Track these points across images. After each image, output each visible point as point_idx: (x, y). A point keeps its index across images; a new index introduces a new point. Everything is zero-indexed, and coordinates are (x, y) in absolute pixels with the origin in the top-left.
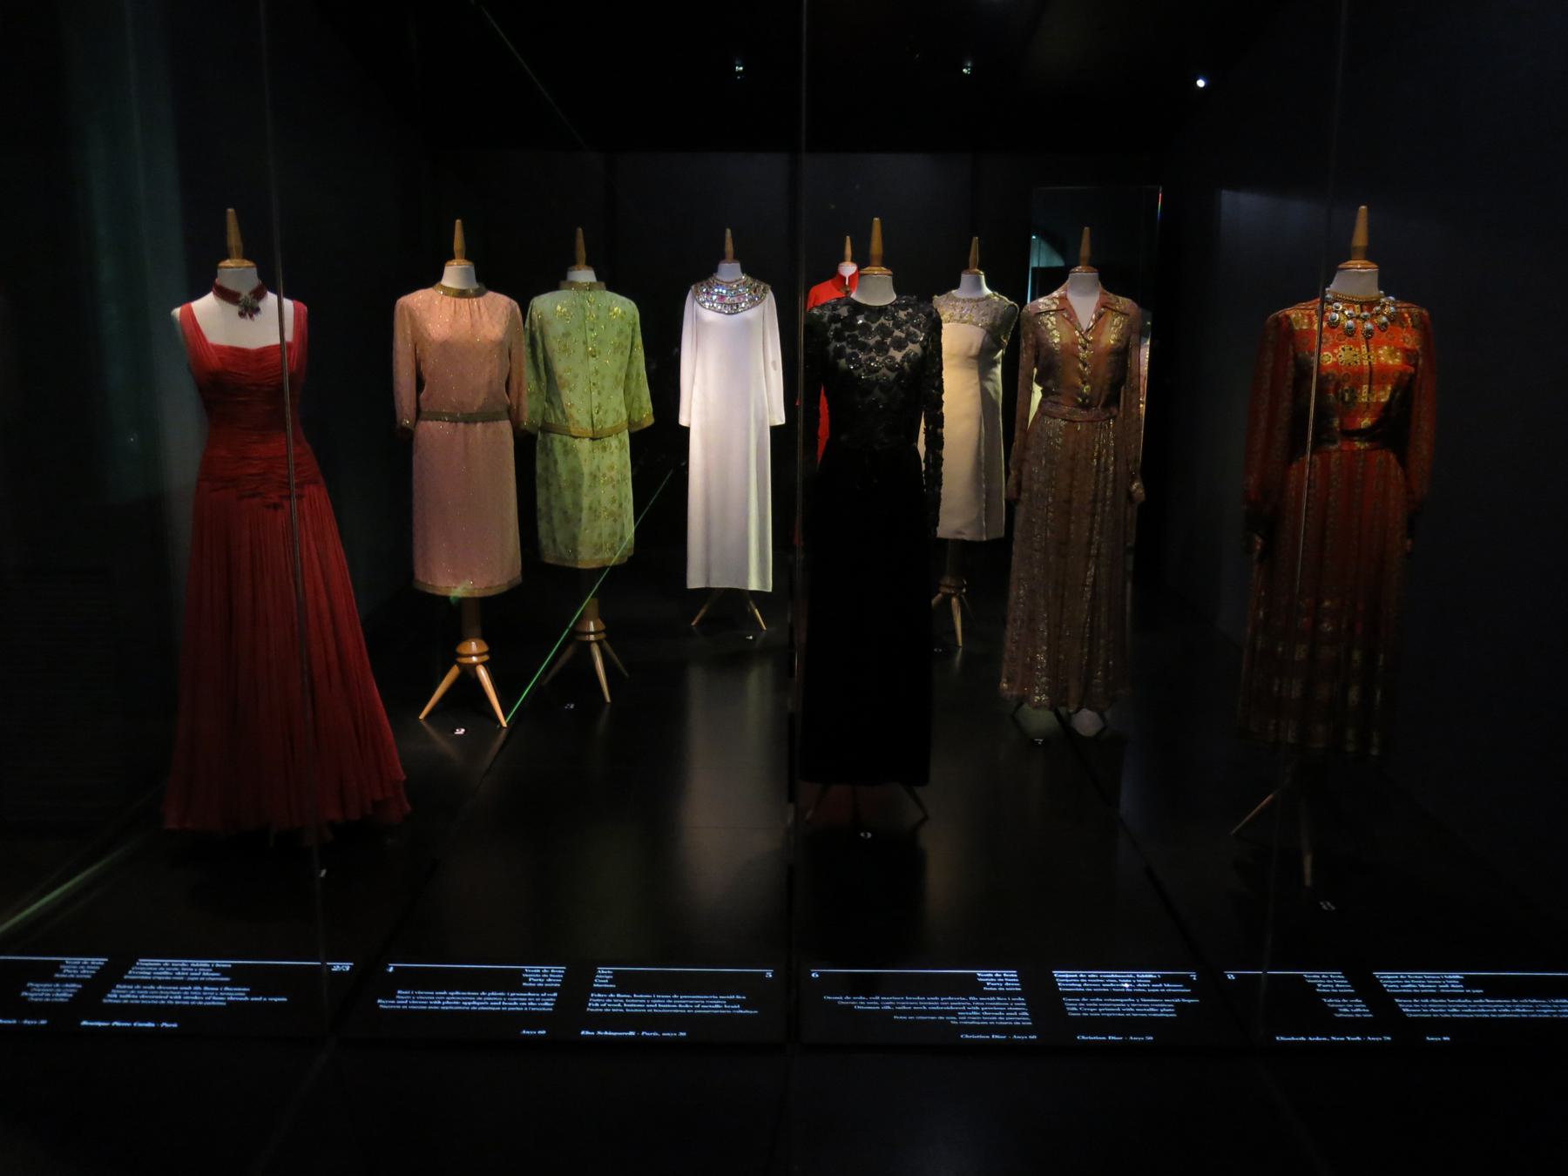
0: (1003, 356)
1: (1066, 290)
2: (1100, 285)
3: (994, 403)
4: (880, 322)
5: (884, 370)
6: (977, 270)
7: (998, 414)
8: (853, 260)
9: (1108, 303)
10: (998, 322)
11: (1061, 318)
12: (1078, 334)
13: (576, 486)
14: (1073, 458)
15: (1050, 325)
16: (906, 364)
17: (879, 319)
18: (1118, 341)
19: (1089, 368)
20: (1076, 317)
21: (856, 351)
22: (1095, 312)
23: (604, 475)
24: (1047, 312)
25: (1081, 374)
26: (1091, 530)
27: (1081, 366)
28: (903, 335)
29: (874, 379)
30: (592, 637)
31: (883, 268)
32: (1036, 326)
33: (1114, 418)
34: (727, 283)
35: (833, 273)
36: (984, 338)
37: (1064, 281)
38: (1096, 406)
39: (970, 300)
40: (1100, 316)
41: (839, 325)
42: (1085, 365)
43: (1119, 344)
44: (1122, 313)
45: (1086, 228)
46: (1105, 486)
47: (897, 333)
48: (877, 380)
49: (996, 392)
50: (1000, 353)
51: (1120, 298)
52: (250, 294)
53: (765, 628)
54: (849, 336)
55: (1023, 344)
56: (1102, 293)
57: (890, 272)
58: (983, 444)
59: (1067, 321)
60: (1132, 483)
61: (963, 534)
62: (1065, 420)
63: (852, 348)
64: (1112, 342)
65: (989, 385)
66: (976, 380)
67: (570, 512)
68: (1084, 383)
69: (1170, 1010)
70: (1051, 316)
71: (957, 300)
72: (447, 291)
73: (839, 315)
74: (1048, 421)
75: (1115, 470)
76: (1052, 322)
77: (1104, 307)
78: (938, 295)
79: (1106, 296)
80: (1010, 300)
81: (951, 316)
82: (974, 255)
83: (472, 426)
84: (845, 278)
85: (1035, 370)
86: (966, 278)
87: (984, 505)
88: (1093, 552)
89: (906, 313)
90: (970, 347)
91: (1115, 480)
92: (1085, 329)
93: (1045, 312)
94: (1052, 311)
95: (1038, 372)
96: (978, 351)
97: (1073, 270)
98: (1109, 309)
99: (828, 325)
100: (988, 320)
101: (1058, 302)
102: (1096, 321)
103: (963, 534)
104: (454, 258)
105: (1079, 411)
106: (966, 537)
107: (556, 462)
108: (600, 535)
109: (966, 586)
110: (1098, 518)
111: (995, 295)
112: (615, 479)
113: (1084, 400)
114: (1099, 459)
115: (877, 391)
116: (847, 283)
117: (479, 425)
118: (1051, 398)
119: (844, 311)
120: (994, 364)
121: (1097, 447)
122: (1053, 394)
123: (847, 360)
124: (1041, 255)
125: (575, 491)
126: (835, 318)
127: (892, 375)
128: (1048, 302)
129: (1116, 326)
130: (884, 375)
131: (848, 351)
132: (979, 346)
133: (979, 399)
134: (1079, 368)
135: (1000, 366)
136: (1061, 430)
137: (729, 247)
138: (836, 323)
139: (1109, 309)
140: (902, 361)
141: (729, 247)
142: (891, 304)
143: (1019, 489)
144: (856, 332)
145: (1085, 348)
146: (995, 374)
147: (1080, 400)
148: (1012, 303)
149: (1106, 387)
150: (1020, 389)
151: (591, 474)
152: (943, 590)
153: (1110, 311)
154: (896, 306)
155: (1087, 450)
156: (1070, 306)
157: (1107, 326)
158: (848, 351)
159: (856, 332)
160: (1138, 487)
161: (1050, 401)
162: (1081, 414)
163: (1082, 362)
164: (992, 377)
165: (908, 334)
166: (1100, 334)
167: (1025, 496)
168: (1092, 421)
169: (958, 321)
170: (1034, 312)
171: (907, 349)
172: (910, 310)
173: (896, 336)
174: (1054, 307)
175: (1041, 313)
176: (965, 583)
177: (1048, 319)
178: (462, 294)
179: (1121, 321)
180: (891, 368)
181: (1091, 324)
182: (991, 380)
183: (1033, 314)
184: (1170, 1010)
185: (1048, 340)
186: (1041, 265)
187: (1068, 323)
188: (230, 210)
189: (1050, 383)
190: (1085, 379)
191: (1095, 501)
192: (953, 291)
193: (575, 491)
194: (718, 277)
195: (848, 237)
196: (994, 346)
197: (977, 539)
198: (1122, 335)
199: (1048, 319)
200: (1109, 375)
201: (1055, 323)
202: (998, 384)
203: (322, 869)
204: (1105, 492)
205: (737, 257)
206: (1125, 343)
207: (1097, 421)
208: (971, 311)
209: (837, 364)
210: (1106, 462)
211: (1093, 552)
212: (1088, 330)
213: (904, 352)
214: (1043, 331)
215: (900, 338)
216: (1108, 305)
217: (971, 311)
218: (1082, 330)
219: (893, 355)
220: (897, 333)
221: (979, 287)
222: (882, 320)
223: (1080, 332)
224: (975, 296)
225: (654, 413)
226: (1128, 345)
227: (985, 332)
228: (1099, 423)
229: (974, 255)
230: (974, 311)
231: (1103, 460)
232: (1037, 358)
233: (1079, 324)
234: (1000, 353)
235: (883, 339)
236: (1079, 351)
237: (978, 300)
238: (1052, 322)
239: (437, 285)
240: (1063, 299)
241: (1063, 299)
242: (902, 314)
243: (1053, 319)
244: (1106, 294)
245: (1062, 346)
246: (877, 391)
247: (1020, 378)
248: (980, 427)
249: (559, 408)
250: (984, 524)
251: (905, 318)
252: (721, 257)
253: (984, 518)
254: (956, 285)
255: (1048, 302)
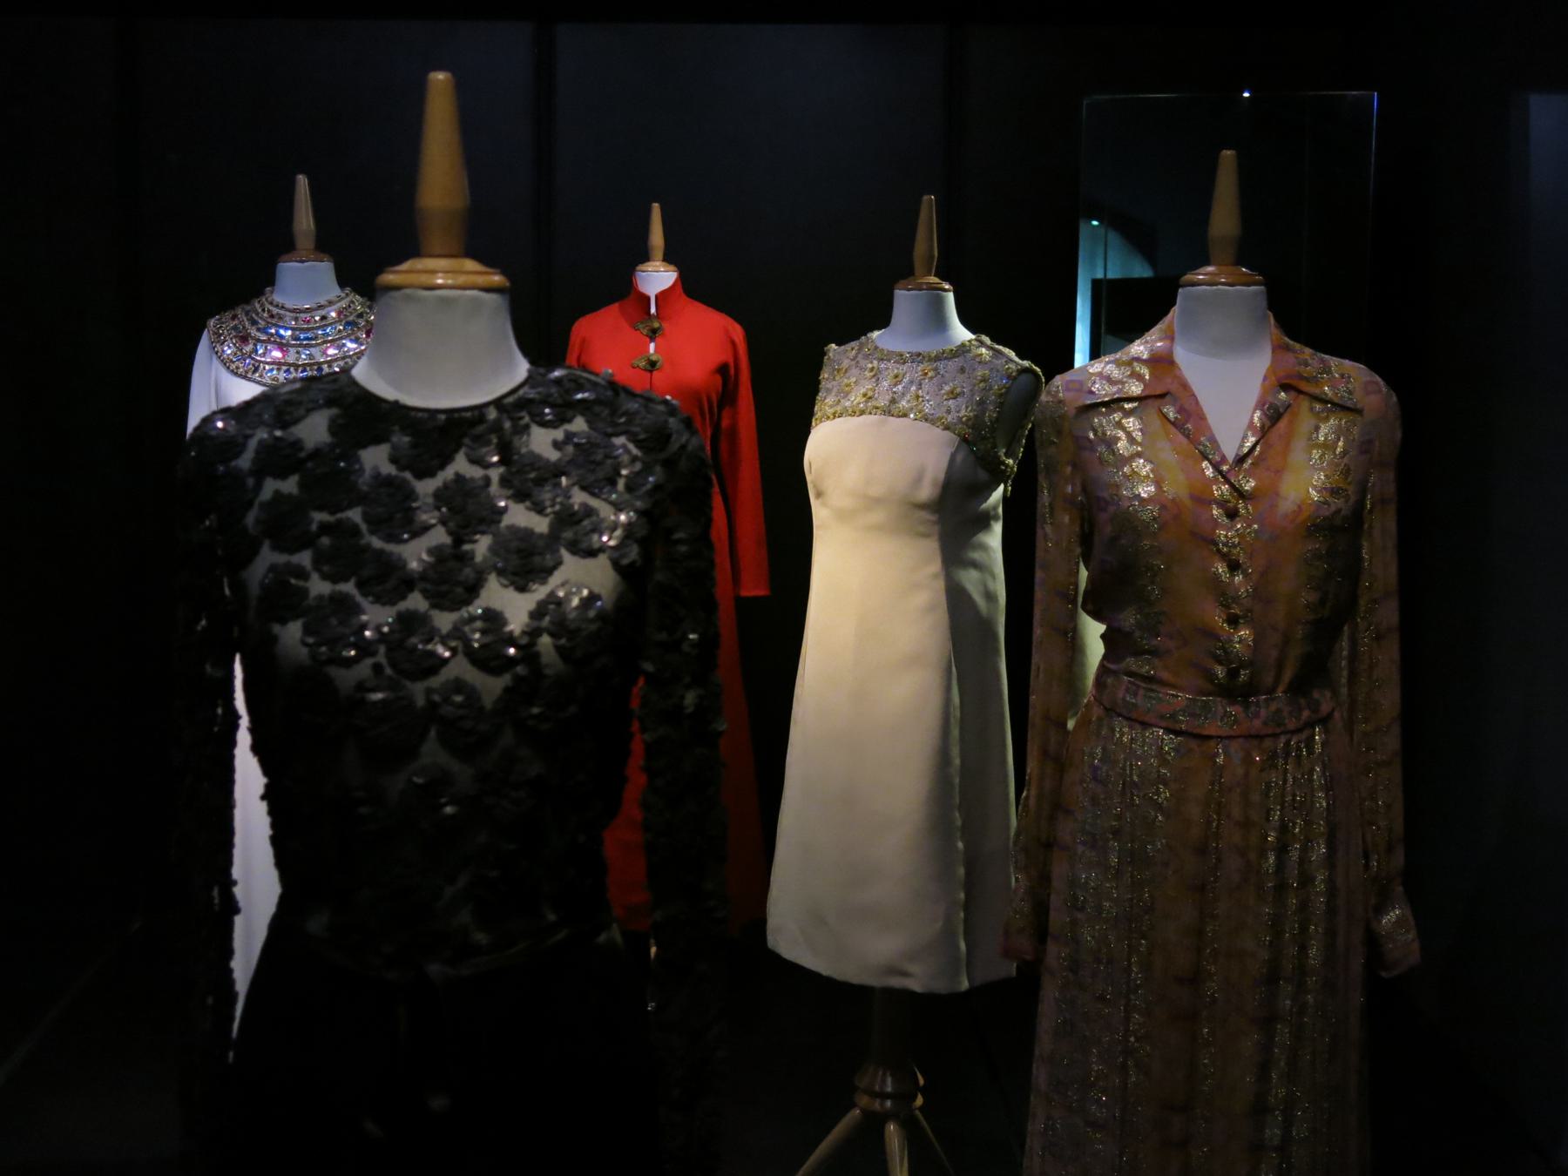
0: (1006, 499)
1: (1170, 337)
2: (1272, 321)
3: (987, 626)
4: (448, 473)
5: (461, 669)
6: (934, 279)
7: (997, 651)
8: (668, 258)
9: (1301, 377)
10: (991, 413)
11: (1156, 422)
12: (1209, 472)
14: (1202, 850)
15: (1122, 445)
16: (545, 640)
17: (446, 460)
18: (1334, 492)
19: (1246, 575)
20: (1202, 418)
21: (349, 587)
22: (1260, 405)
24: (1114, 404)
25: (1223, 595)
26: (1264, 1069)
27: (1221, 568)
28: (541, 525)
29: (420, 701)
31: (470, 264)
32: (1082, 444)
33: (1324, 721)
34: (294, 311)
35: (623, 289)
36: (953, 457)
37: (1166, 313)
38: (1271, 691)
39: (917, 357)
40: (1274, 416)
41: (290, 485)
42: (1234, 567)
43: (1338, 503)
44: (1341, 407)
45: (1228, 154)
46: (1304, 929)
47: (519, 516)
48: (432, 706)
49: (990, 597)
50: (998, 493)
51: (1334, 361)
54: (325, 528)
55: (1045, 497)
56: (1278, 348)
57: (497, 279)
58: (955, 732)
59: (1173, 429)
60: (1380, 910)
61: (905, 974)
62: (1178, 733)
63: (334, 579)
64: (1314, 495)
65: (970, 579)
66: (936, 566)
68: (1233, 621)
70: (1128, 414)
71: (885, 357)
73: (297, 444)
74: (1124, 733)
75: (1330, 882)
76: (1129, 435)
77: (1285, 387)
78: (839, 344)
79: (1290, 357)
80: (1022, 358)
81: (868, 398)
82: (926, 242)
84: (648, 299)
85: (1084, 574)
86: (904, 300)
87: (962, 896)
88: (1273, 1133)
89: (559, 434)
90: (918, 480)
91: (1331, 910)
92: (1231, 456)
93: (1104, 404)
94: (1130, 399)
95: (1090, 579)
96: (937, 491)
97: (1189, 277)
98: (1300, 392)
99: (251, 482)
100: (962, 410)
101: (1145, 372)
102: (1264, 433)
103: (905, 974)
105: (1219, 705)
106: (915, 986)
109: (924, 1091)
110: (1283, 1033)
111: (982, 344)
113: (1233, 674)
114: (1282, 849)
115: (432, 752)
116: (653, 310)
118: (1131, 663)
119: (315, 430)
120: (984, 522)
121: (1276, 816)
122: (1139, 653)
123: (307, 630)
124: (1110, 253)
126: (280, 459)
127: (491, 687)
128: (1116, 373)
129: (1328, 446)
130: (459, 685)
131: (319, 587)
132: (942, 476)
133: (942, 615)
134: (1217, 576)
135: (998, 528)
136: (1164, 762)
137: (304, 220)
138: (282, 475)
139: (1300, 392)
140: (533, 633)
141: (304, 220)
142: (498, 403)
143: (1057, 807)
144: (355, 515)
145: (1232, 514)
146: (984, 548)
147: (1220, 671)
148: (1026, 363)
149: (1299, 632)
150: (1038, 632)
152: (863, 1100)
153: (1305, 404)
154: (515, 407)
155: (1246, 824)
156: (1185, 386)
157: (1299, 444)
158: (319, 587)
159: (355, 515)
160: (1399, 922)
161: (1130, 674)
162: (1223, 717)
163: (1225, 557)
164: (976, 555)
165: (567, 519)
166: (1279, 472)
167: (1055, 953)
168: (1260, 737)
169: (887, 412)
170: (1075, 400)
171: (556, 579)
172: (579, 425)
173: (513, 529)
174: (1136, 389)
175: (1095, 406)
176: (922, 1082)
177: (1119, 425)
179: (1339, 432)
180: (488, 660)
181: (1252, 440)
182: (975, 565)
183: (1070, 410)
185: (1118, 486)
186: (1110, 275)
187: (1181, 438)
189: (1129, 619)
190: (1236, 610)
191: (1272, 978)
192: (875, 334)
194: (277, 298)
196: (983, 475)
197: (941, 986)
198: (1346, 472)
199: (1119, 425)
200: (1308, 597)
201: (1138, 436)
202: (993, 577)
203: (689, 639)
204: (1303, 948)
206: (1353, 499)
207: (1275, 736)
208: (920, 386)
209: (274, 639)
210: (1303, 861)
211: (1273, 1133)
212: (1241, 460)
213: (540, 592)
214: (1101, 460)
215: (527, 534)
216: (1294, 382)
217: (920, 386)
218: (1224, 460)
219: (496, 605)
220: (519, 516)
221: (941, 324)
222: (460, 465)
223: (1216, 467)
224: (929, 346)
225: (816, 391)
226: (1361, 503)
227: (956, 439)
228: (1283, 739)
229: (926, 242)
230: (926, 385)
231: (1294, 855)
232: (1086, 540)
233: (1213, 440)
234: (998, 493)
235: (458, 541)
236: (1215, 524)
237: (938, 358)
238: (1129, 435)
240: (1162, 363)
241: (1162, 363)
242: (542, 442)
243: (1131, 423)
244: (1287, 348)
245: (1163, 507)
246: (432, 752)
247: (1039, 594)
248: (948, 689)
250: (963, 946)
251: (553, 455)
252: (286, 246)
253: (961, 929)
254: (882, 320)
255: (1116, 373)
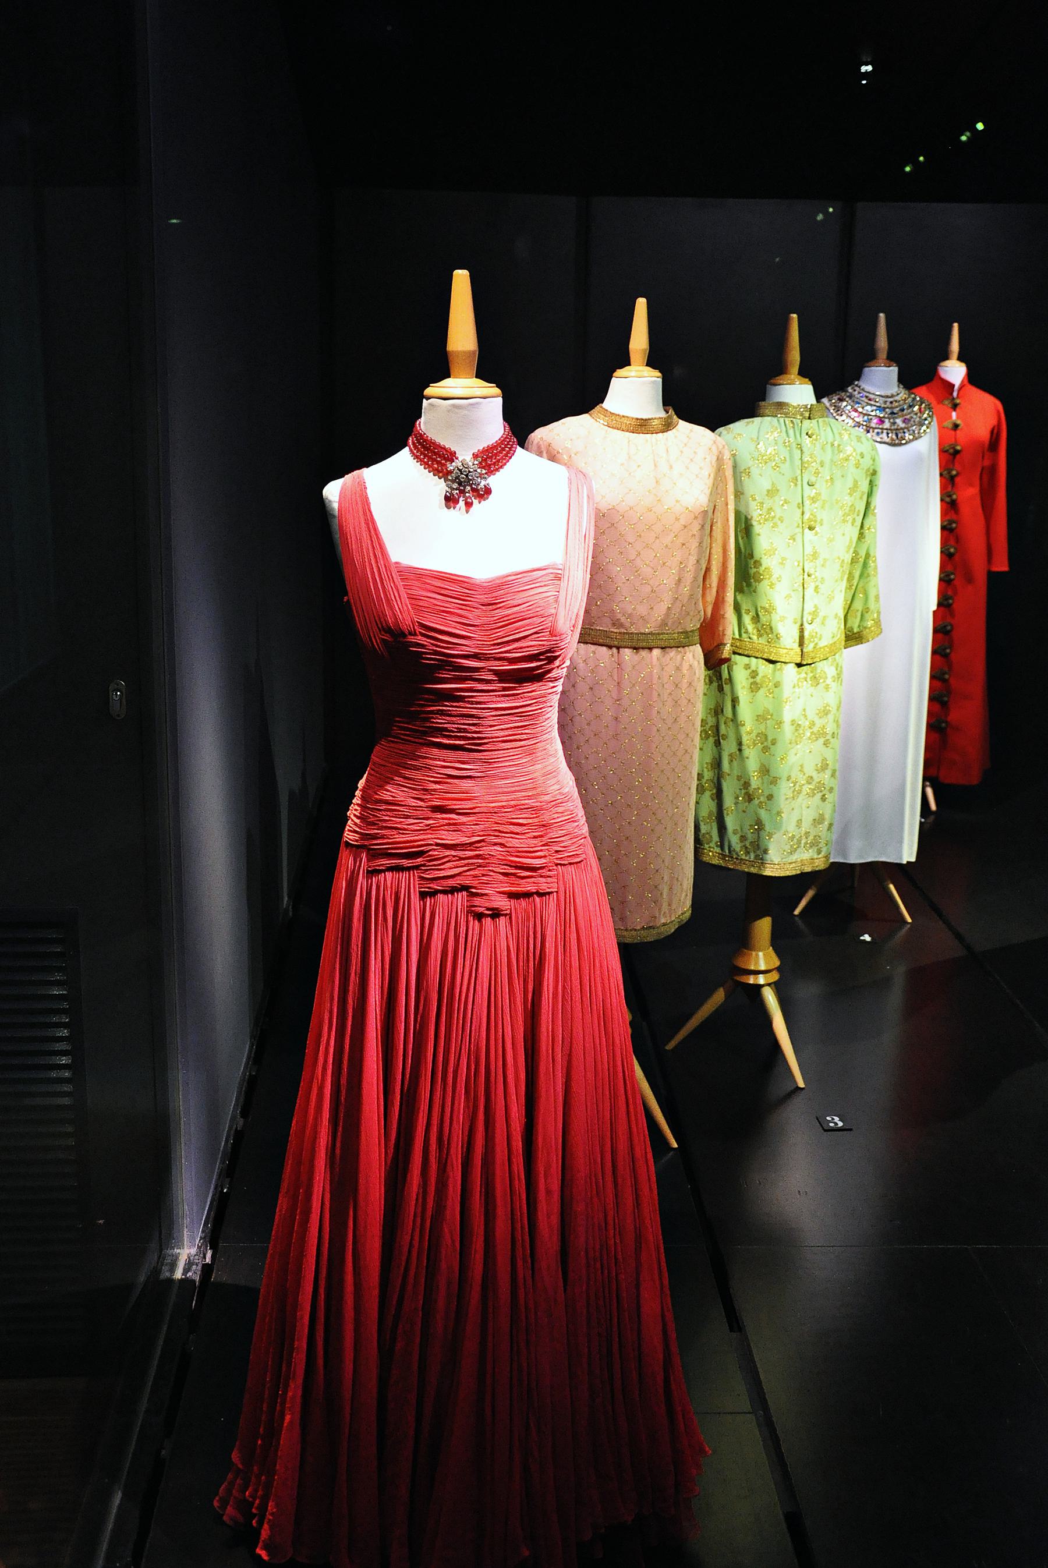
13: (767, 744)
23: (813, 724)
30: (761, 980)
52: (475, 456)
53: (909, 920)
67: (755, 782)
69: (412, 875)
72: (618, 423)
83: (644, 653)
104: (628, 363)
107: (735, 701)
108: (799, 823)
112: (829, 730)
117: (656, 652)
125: (765, 749)
151: (793, 722)
178: (642, 426)
184: (412, 875)
188: (882, 315)
193: (765, 749)
195: (956, 325)
205: (892, 358)
239: (598, 408)
249: (748, 612)
252: (869, 357)
